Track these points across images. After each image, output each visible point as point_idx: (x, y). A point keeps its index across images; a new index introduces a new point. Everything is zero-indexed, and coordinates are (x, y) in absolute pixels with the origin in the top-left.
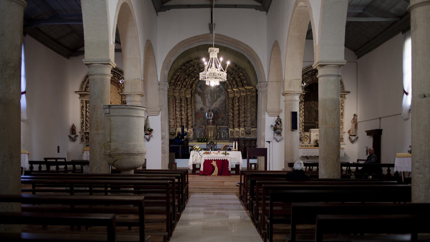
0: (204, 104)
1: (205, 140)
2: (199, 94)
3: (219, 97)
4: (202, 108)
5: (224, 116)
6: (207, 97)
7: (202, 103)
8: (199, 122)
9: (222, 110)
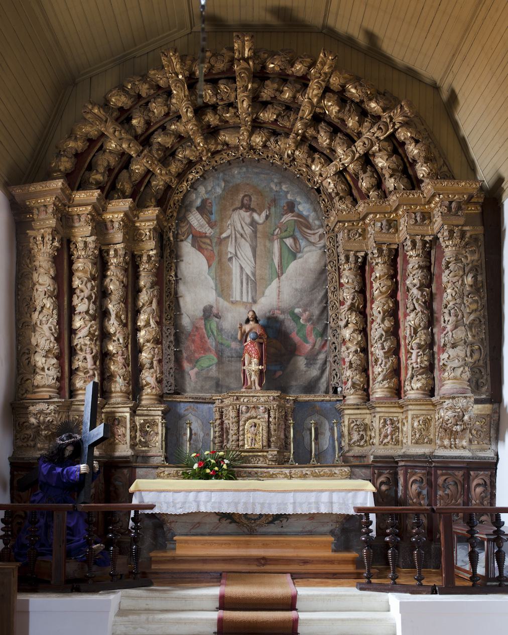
0: (223, 289)
1: (220, 467)
2: (199, 241)
3: (294, 256)
4: (211, 307)
5: (317, 347)
6: (236, 255)
7: (212, 283)
8: (197, 374)
9: (309, 319)
